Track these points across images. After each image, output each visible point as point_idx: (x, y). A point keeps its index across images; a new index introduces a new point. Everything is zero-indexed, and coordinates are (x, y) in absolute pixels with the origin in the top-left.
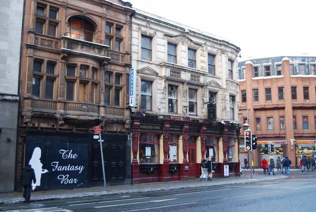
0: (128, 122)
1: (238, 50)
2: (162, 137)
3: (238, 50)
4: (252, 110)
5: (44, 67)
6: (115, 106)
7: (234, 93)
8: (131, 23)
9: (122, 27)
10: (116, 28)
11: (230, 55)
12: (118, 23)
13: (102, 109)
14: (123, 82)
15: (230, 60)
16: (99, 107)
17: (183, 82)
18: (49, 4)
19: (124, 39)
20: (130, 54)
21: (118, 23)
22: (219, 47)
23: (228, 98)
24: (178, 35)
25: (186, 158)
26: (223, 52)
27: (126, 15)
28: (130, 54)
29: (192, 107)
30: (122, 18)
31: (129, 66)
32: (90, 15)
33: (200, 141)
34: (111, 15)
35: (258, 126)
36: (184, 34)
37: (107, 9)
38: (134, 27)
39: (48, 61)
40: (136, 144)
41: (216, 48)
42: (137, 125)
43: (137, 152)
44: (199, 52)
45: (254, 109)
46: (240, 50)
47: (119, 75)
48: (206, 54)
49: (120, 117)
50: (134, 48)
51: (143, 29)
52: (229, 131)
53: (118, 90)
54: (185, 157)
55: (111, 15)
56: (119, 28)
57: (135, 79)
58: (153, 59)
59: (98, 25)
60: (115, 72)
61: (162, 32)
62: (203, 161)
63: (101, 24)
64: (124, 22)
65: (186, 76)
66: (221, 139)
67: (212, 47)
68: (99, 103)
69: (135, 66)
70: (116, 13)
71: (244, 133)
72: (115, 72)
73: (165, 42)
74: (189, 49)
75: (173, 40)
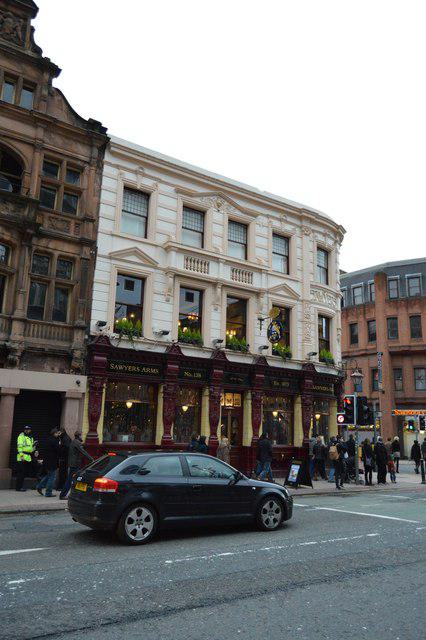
0: (77, 354)
1: (338, 232)
2: (207, 392)
3: (338, 232)
4: (386, 355)
5: (54, 267)
6: (55, 323)
7: (329, 311)
8: (100, 166)
9: (82, 169)
10: (68, 170)
11: (320, 238)
12: (71, 160)
13: (17, 327)
14: (75, 274)
15: (320, 248)
16: (10, 320)
17: (214, 284)
18: (65, 161)
19: (84, 194)
20: (93, 221)
21: (71, 160)
22: (297, 222)
23: (314, 319)
24: (203, 195)
25: (95, 431)
26: (305, 233)
27: (92, 146)
28: (93, 221)
29: (192, 326)
30: (82, 152)
31: (92, 244)
32: (8, 140)
33: (207, 399)
34: (56, 143)
35: (399, 384)
36: (224, 191)
37: (45, 130)
38: (107, 169)
39: (60, 256)
40: (259, 413)
41: (291, 224)
42: (101, 362)
43: (259, 427)
44: (254, 229)
45: (390, 353)
46: (344, 232)
47: (67, 261)
48: (312, 246)
49: (64, 345)
50: (104, 210)
51: (276, 224)
52: (316, 384)
53: (65, 291)
54: (167, 432)
55: (56, 143)
56: (75, 172)
57: (104, 275)
58: (206, 248)
59: (27, 165)
60: (57, 254)
61: (173, 185)
62: (306, 444)
63: (34, 163)
64: (87, 159)
65: (220, 273)
66: (299, 399)
67: (280, 220)
68: (13, 314)
69: (105, 245)
70: (67, 141)
71: (348, 394)
72: (57, 254)
73: (176, 204)
74: (231, 221)
75: (197, 202)
